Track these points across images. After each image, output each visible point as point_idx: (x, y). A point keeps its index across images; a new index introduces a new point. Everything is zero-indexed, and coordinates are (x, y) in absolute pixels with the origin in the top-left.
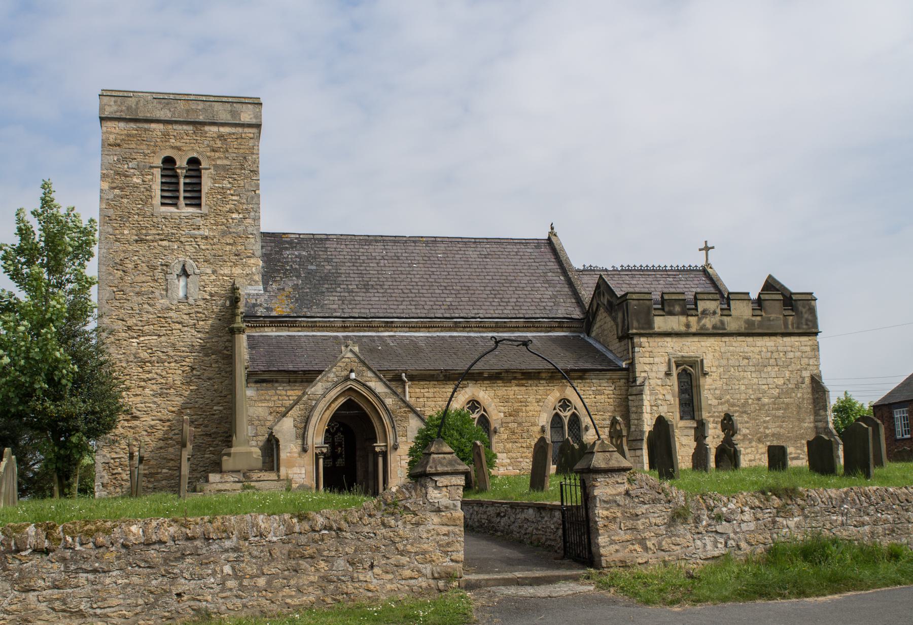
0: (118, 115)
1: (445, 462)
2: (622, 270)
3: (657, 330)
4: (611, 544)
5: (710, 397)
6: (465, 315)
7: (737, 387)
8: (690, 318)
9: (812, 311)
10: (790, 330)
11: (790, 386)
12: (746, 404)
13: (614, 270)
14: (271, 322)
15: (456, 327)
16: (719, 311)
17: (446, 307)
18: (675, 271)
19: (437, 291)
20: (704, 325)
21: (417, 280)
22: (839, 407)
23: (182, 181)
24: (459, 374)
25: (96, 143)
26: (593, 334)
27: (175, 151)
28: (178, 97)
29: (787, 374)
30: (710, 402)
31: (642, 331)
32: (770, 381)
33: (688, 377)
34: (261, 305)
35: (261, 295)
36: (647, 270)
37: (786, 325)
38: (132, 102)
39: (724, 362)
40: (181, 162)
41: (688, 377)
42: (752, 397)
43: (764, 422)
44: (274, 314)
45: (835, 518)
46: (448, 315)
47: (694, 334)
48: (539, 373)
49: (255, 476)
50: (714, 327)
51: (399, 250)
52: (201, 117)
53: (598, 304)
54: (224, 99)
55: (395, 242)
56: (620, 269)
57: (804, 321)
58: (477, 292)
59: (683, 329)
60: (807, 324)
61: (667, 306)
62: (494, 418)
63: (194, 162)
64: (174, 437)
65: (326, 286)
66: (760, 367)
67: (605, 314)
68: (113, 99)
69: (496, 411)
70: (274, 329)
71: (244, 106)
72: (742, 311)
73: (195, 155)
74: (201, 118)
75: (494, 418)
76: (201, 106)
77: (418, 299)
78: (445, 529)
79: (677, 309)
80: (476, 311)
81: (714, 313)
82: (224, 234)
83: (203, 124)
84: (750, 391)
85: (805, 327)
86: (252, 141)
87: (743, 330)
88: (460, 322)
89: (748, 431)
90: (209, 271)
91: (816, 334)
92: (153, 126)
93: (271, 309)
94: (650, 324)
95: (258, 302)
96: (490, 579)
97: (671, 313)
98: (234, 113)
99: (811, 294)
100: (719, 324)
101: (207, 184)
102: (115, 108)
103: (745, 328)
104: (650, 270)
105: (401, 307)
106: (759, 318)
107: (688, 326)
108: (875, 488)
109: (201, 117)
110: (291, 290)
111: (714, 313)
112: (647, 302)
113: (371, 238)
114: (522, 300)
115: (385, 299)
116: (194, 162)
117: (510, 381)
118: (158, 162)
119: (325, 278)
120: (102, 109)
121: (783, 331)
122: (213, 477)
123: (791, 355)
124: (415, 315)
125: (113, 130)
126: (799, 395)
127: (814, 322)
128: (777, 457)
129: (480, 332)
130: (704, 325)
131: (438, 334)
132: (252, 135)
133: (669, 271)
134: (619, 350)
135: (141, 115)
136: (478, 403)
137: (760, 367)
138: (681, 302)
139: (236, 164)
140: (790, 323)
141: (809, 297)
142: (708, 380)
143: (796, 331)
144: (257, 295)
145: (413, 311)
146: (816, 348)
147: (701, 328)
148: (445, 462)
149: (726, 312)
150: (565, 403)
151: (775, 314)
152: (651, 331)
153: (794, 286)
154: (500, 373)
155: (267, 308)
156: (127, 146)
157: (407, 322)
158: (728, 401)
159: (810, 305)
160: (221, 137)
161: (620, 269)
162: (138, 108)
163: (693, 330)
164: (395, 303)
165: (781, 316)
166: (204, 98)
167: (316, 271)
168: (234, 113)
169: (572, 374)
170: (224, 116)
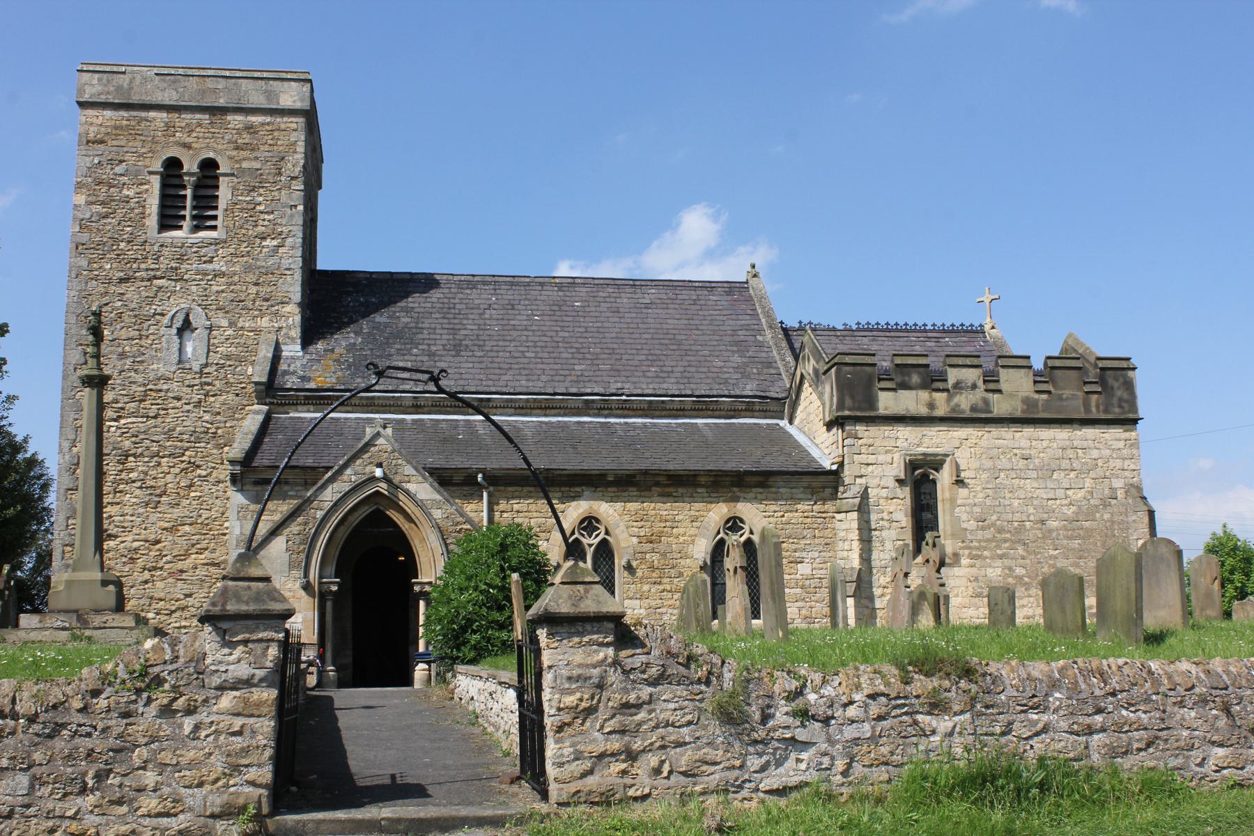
0: (103, 99)
1: (245, 595)
2: (858, 330)
3: (882, 411)
4: (577, 759)
5: (964, 517)
6: (601, 390)
7: (1007, 502)
8: (937, 395)
9: (1129, 386)
10: (1094, 414)
11: (1092, 502)
12: (1020, 529)
13: (845, 330)
14: (306, 398)
15: (587, 408)
16: (980, 383)
17: (574, 378)
18: (939, 331)
19: (564, 355)
20: (957, 405)
21: (536, 339)
22: (1214, 546)
23: (188, 193)
24: (568, 475)
25: (69, 137)
26: (797, 421)
27: (184, 151)
28: (190, 72)
29: (1088, 483)
30: (964, 525)
31: (859, 414)
32: (1060, 493)
33: (920, 479)
34: (294, 373)
35: (298, 358)
36: (897, 330)
37: (1087, 409)
38: (124, 80)
39: (988, 464)
40: (190, 166)
41: (920, 479)
42: (1032, 518)
43: (1051, 557)
44: (312, 385)
45: (1035, 717)
46: (574, 390)
47: (942, 420)
48: (695, 476)
49: (97, 620)
50: (973, 409)
51: (508, 295)
52: (222, 101)
53: (802, 375)
54: (256, 75)
55: (512, 284)
56: (854, 327)
57: (1115, 401)
58: (625, 357)
59: (923, 411)
60: (1120, 406)
61: (904, 374)
62: (623, 545)
63: (209, 166)
64: (167, 566)
65: (398, 346)
66: (1046, 472)
67: (810, 390)
68: (97, 76)
69: (626, 535)
70: (312, 408)
71: (286, 84)
72: (1017, 385)
73: (211, 155)
74: (222, 102)
75: (623, 545)
76: (222, 84)
77: (531, 366)
78: (238, 723)
79: (915, 379)
80: (619, 385)
81: (974, 387)
82: (248, 269)
83: (224, 111)
84: (1031, 510)
85: (1117, 410)
86: (295, 134)
87: (1018, 414)
88: (593, 401)
89: (1024, 571)
90: (225, 323)
91: (1135, 421)
92: (152, 114)
93: (309, 379)
94: (871, 403)
95: (292, 369)
96: (324, 821)
97: (905, 386)
98: (269, 95)
99: (1128, 359)
100: (981, 404)
101: (224, 193)
102: (100, 88)
103: (1023, 411)
104: (901, 331)
105: (504, 378)
106: (1044, 396)
107: (931, 406)
108: (1121, 661)
109: (222, 101)
110: (343, 351)
111: (974, 387)
112: (868, 368)
113: (476, 279)
114: (693, 369)
115: (483, 366)
116: (209, 166)
117: (649, 489)
118: (157, 166)
119: (398, 335)
120: (81, 91)
121: (1083, 416)
122: (25, 620)
123: (1095, 454)
124: (524, 390)
125: (95, 120)
126: (1106, 516)
127: (1132, 403)
128: (1001, 603)
129: (625, 417)
130: (957, 405)
131: (560, 419)
132: (294, 126)
133: (930, 331)
134: (827, 444)
135: (135, 99)
136: (598, 521)
137: (1046, 472)
138: (921, 370)
139: (268, 169)
140: (1093, 404)
141: (1124, 364)
142: (894, 473)
143: (1103, 416)
144: (292, 358)
145: (523, 384)
146: (1135, 444)
147: (953, 410)
148: (245, 595)
149: (992, 386)
150: (734, 524)
151: (1072, 396)
152: (873, 414)
153: (1102, 345)
154: (633, 476)
155: (303, 378)
156: (115, 143)
157: (511, 400)
158: (993, 525)
159: (1125, 377)
160: (249, 128)
161: (854, 327)
162: (131, 88)
163: (941, 411)
164: (497, 371)
165: (1080, 394)
166: (227, 74)
167: (386, 325)
168: (269, 95)
169: (748, 479)
170: (257, 100)
